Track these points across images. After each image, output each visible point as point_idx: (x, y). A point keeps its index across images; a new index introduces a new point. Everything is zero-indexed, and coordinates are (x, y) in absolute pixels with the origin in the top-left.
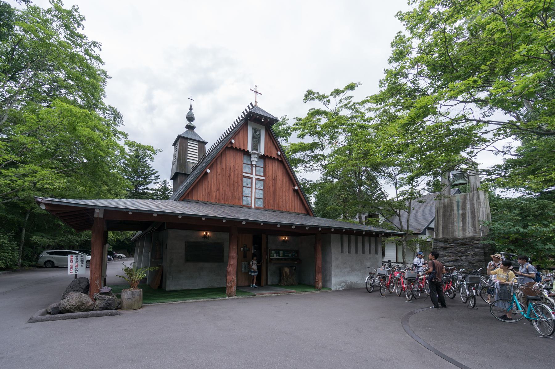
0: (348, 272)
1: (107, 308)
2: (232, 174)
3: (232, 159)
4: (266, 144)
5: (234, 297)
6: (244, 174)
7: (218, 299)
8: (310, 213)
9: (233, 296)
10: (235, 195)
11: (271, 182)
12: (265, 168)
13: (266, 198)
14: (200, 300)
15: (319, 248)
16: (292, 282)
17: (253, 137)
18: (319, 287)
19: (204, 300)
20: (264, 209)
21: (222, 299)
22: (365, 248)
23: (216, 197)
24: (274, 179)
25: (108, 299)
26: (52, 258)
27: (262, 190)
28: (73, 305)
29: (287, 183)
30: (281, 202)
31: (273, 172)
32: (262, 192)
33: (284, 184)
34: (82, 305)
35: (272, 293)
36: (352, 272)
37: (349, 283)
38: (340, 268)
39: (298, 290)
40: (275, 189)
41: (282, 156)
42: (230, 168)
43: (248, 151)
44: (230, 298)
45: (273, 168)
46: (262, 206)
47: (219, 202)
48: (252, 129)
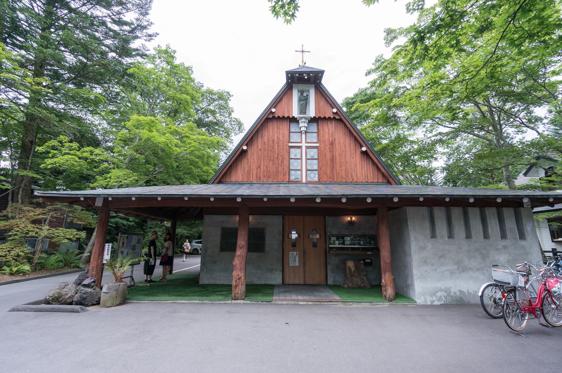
0: (452, 273)
1: (81, 302)
2: (276, 147)
3: (276, 130)
4: (317, 104)
5: (239, 301)
6: (290, 144)
7: (217, 302)
8: (391, 180)
9: (239, 300)
10: (280, 170)
11: (327, 148)
12: (318, 133)
13: (321, 169)
14: (195, 302)
15: (537, 230)
16: (360, 283)
17: (300, 100)
18: (388, 296)
19: (199, 302)
20: (319, 182)
21: (222, 302)
22: (489, 227)
23: (256, 175)
24: (332, 144)
25: (83, 292)
26: (197, 246)
27: (317, 159)
28: (51, 297)
29: (352, 146)
30: (344, 171)
31: (330, 135)
32: (316, 162)
33: (347, 147)
34: (61, 297)
35: (298, 300)
36: (461, 272)
37: (455, 293)
38: (432, 265)
39: (345, 298)
40: (333, 155)
41: (339, 113)
42: (273, 141)
43: (293, 117)
44: (234, 302)
45: (329, 130)
46: (316, 179)
47: (260, 181)
48: (298, 91)
